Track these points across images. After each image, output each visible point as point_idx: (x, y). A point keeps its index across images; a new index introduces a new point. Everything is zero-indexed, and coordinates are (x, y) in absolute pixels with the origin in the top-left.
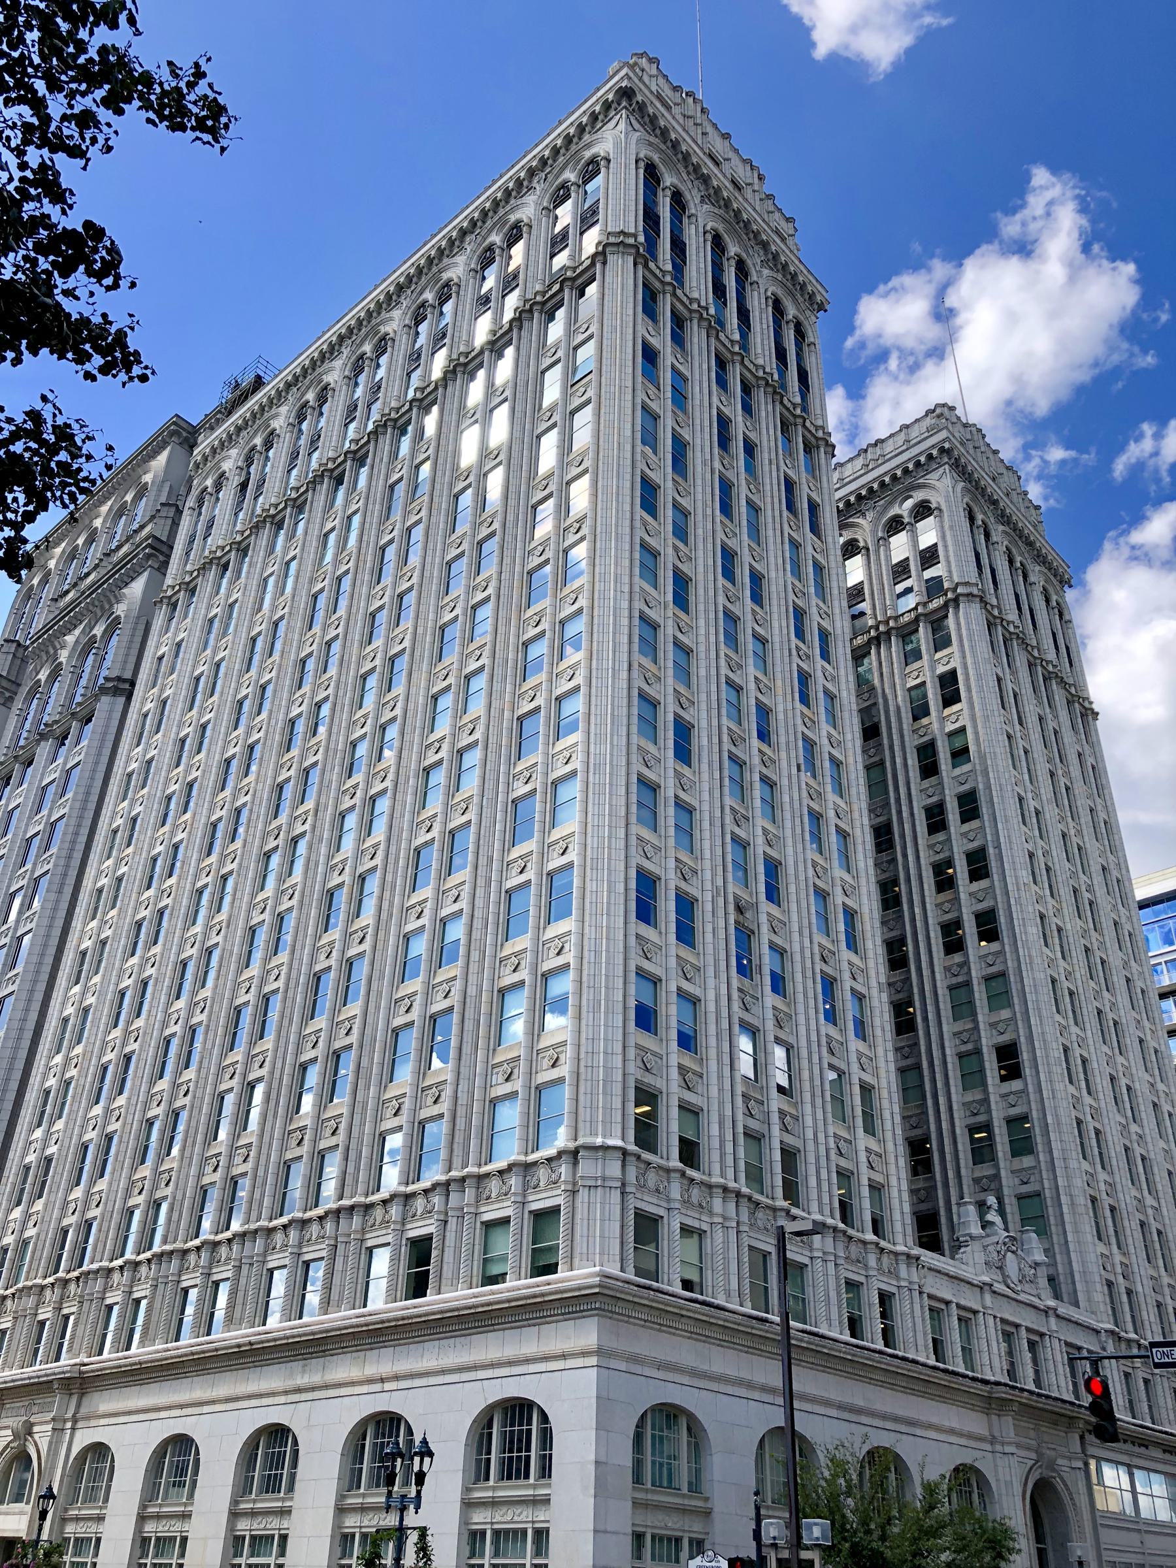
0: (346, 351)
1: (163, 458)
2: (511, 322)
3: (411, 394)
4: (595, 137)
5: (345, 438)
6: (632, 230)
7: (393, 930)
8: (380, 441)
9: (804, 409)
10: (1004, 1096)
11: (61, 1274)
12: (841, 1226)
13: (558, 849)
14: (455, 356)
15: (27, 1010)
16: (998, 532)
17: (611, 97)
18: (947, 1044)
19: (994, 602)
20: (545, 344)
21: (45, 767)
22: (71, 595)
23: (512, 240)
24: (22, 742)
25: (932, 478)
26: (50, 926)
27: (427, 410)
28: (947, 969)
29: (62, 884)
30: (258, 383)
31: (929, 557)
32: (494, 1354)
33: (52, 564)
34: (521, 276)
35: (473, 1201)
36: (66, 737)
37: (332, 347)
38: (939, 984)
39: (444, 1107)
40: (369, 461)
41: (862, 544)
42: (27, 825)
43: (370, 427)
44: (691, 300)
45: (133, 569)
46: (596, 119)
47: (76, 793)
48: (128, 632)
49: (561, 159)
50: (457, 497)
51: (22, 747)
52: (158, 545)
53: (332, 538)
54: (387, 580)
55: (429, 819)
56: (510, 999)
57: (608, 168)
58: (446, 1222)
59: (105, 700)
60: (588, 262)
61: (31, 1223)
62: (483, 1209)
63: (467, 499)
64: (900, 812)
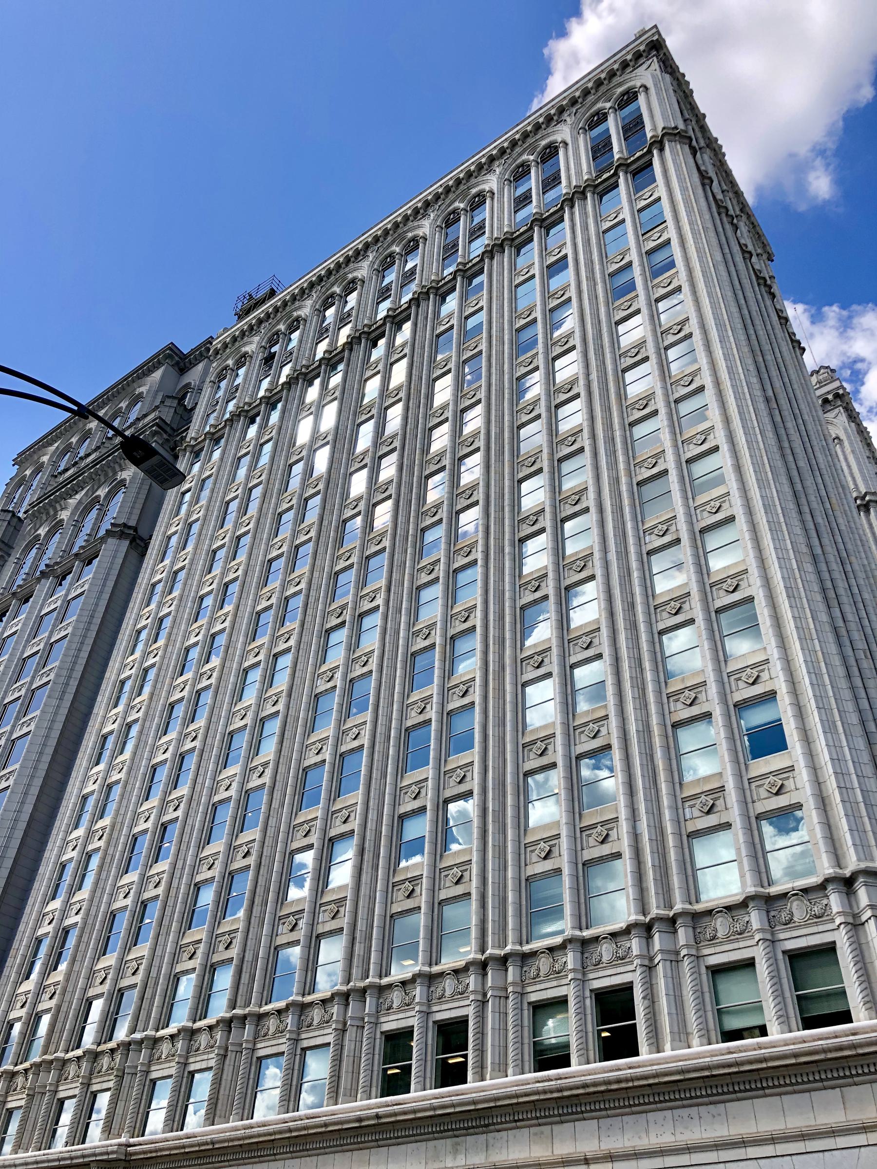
0: (371, 256)
1: (157, 375)
2: (344, 345)
3: (261, 393)
4: (356, 265)
7: (125, 830)
8: (293, 389)
14: (298, 368)
17: (541, 120)
21: (45, 600)
23: (292, 329)
26: (50, 729)
30: (272, 293)
32: (767, 1125)
34: (354, 313)
36: (64, 578)
37: (302, 291)
40: (223, 441)
42: (25, 647)
43: (227, 416)
45: (78, 484)
46: (227, 347)
49: (228, 350)
50: (291, 466)
52: (162, 424)
54: (229, 525)
56: (338, 847)
57: (305, 325)
58: (225, 1056)
59: (111, 541)
60: (381, 322)
62: (435, 1009)
63: (298, 469)
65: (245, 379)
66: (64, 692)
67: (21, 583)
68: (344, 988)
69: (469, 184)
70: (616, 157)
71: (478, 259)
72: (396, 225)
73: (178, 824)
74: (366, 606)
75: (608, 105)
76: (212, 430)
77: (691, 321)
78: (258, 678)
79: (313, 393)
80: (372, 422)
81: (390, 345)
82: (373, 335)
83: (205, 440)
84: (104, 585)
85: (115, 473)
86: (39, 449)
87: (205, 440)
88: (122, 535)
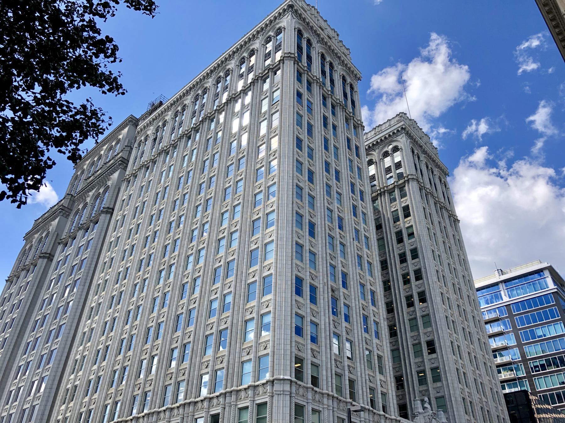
1: (126, 130)
6: (293, 52)
9: (353, 114)
10: (430, 360)
12: (371, 409)
13: (267, 268)
14: (231, 95)
16: (422, 157)
18: (408, 340)
19: (422, 181)
23: (251, 55)
24: (72, 231)
25: (399, 138)
28: (408, 313)
30: (161, 104)
31: (398, 165)
33: (85, 167)
35: (235, 400)
36: (88, 229)
37: (187, 92)
38: (405, 318)
39: (224, 365)
41: (374, 161)
42: (73, 261)
44: (314, 76)
47: (91, 249)
48: (112, 191)
52: (124, 160)
53: (186, 158)
54: (206, 172)
59: (41, 260)
64: (390, 256)
65: (207, 100)
66: (85, 283)
67: (65, 237)
68: (271, 379)
69: (276, 23)
72: (271, 22)
73: (196, 310)
74: (233, 229)
76: (195, 126)
78: (225, 244)
79: (238, 107)
80: (266, 121)
81: (272, 82)
82: (275, 69)
83: (191, 131)
85: (106, 182)
88: (44, 257)
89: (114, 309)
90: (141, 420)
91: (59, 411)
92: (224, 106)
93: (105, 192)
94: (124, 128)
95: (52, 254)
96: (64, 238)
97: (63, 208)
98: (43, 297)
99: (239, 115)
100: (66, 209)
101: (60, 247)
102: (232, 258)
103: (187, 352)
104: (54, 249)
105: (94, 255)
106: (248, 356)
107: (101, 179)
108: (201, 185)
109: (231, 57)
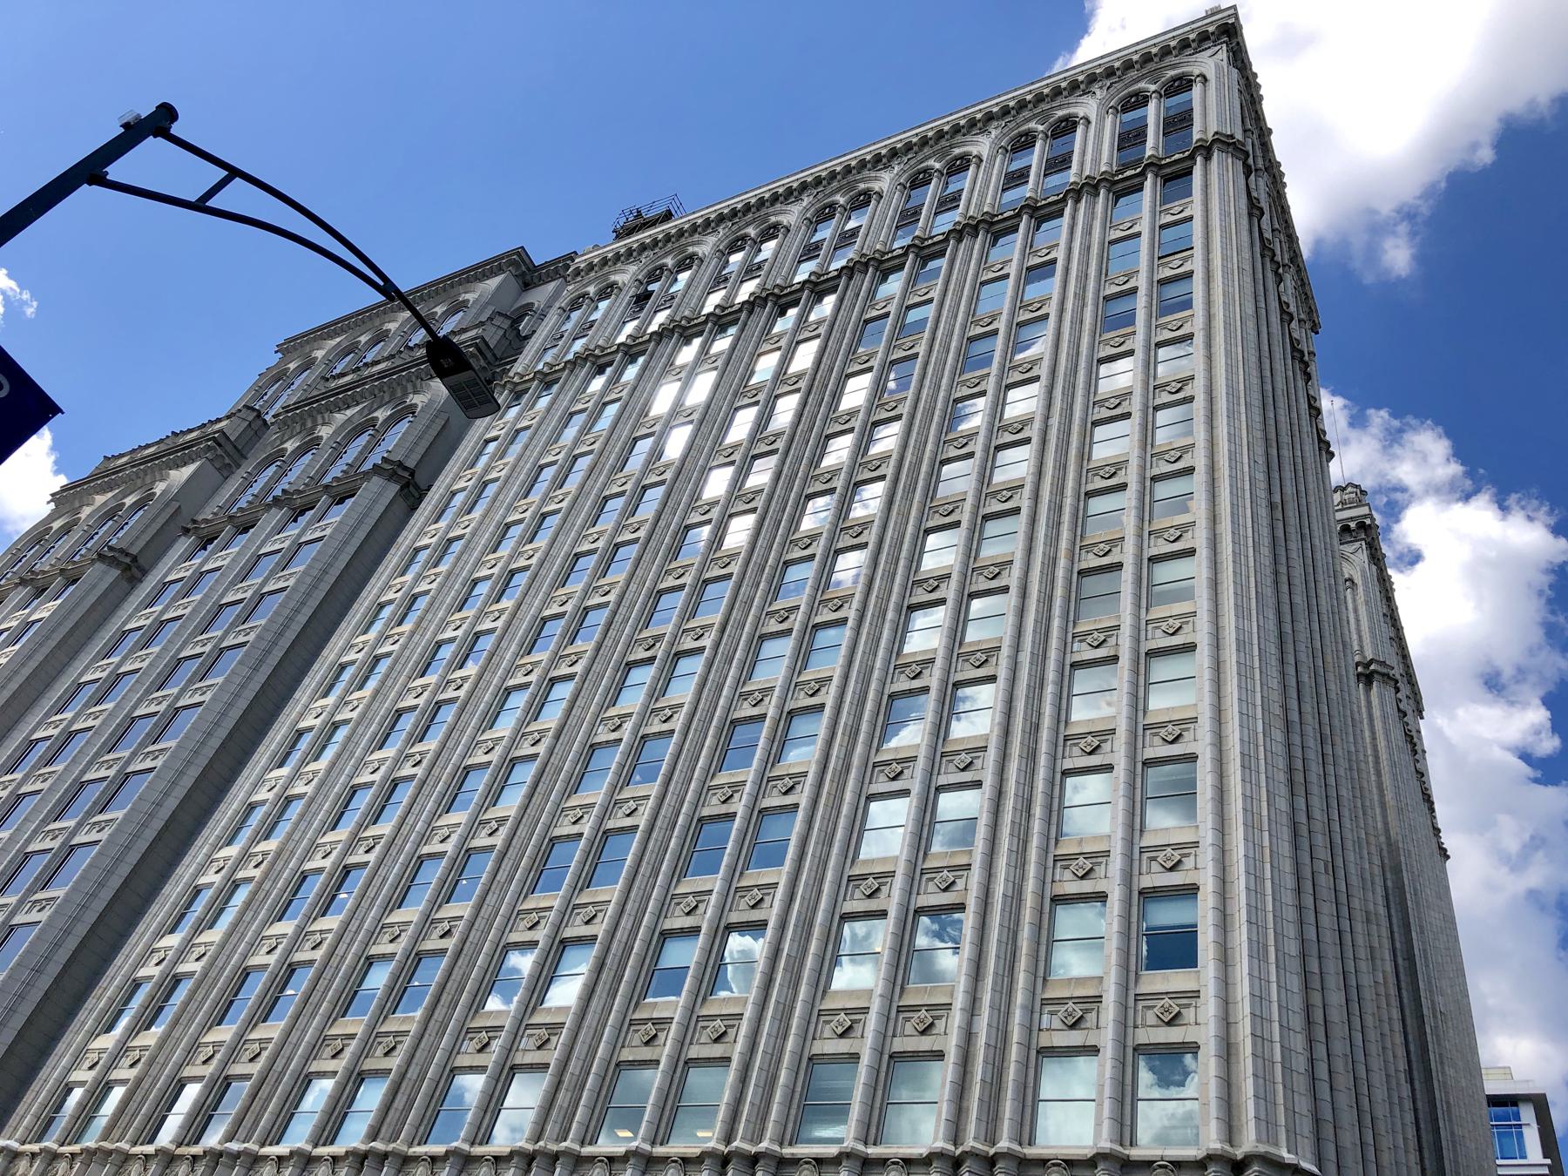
1: (493, 283)
2: (652, 334)
5: (540, 360)
11: (50, 1143)
14: (678, 318)
15: (166, 794)
20: (584, 391)
22: (194, 435)
23: (682, 266)
24: (77, 558)
27: (633, 359)
29: (261, 661)
30: (668, 216)
33: (319, 354)
36: (210, 541)
37: (707, 223)
39: (394, 1062)
40: (556, 388)
47: (310, 567)
48: (155, 511)
51: (75, 563)
52: (483, 348)
54: (535, 497)
55: (539, 732)
56: (571, 954)
61: (127, 1062)
63: (644, 446)
65: (605, 316)
69: (954, 141)
70: (1149, 153)
71: (941, 237)
73: (366, 872)
75: (1153, 87)
76: (546, 370)
77: (1195, 381)
81: (802, 319)
82: (784, 300)
83: (533, 379)
84: (352, 534)
86: (315, 339)
87: (533, 379)
88: (392, 476)
89: (401, 752)
90: (62, 1166)
91: (82, 1051)
92: (649, 341)
93: (301, 451)
94: (493, 273)
95: (420, 479)
96: (206, 521)
97: (222, 441)
98: (81, 675)
99: (683, 375)
100: (229, 448)
101: (183, 544)
102: (486, 758)
103: (289, 992)
104: (159, 545)
105: (315, 587)
106: (335, 1061)
107: (389, 385)
108: (508, 526)
109: (790, 195)
